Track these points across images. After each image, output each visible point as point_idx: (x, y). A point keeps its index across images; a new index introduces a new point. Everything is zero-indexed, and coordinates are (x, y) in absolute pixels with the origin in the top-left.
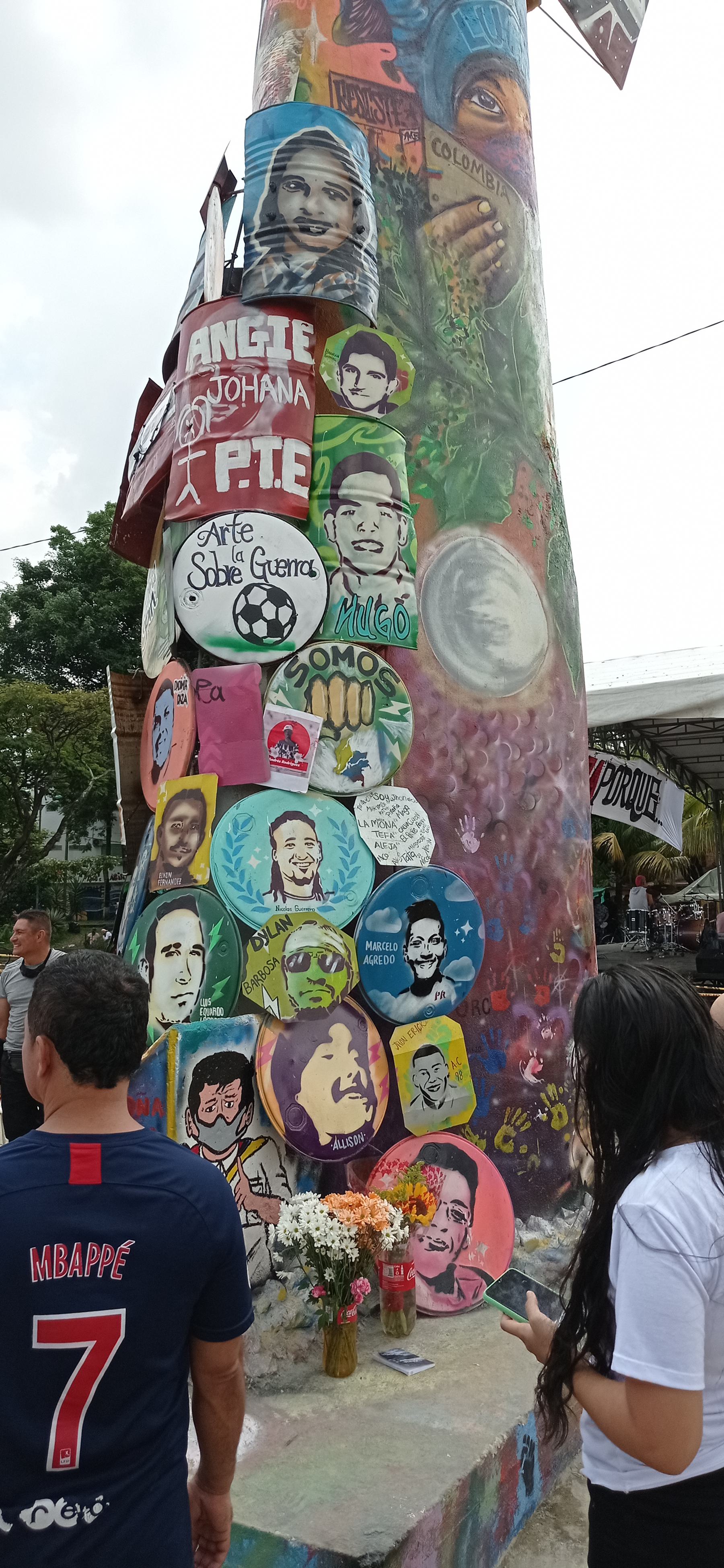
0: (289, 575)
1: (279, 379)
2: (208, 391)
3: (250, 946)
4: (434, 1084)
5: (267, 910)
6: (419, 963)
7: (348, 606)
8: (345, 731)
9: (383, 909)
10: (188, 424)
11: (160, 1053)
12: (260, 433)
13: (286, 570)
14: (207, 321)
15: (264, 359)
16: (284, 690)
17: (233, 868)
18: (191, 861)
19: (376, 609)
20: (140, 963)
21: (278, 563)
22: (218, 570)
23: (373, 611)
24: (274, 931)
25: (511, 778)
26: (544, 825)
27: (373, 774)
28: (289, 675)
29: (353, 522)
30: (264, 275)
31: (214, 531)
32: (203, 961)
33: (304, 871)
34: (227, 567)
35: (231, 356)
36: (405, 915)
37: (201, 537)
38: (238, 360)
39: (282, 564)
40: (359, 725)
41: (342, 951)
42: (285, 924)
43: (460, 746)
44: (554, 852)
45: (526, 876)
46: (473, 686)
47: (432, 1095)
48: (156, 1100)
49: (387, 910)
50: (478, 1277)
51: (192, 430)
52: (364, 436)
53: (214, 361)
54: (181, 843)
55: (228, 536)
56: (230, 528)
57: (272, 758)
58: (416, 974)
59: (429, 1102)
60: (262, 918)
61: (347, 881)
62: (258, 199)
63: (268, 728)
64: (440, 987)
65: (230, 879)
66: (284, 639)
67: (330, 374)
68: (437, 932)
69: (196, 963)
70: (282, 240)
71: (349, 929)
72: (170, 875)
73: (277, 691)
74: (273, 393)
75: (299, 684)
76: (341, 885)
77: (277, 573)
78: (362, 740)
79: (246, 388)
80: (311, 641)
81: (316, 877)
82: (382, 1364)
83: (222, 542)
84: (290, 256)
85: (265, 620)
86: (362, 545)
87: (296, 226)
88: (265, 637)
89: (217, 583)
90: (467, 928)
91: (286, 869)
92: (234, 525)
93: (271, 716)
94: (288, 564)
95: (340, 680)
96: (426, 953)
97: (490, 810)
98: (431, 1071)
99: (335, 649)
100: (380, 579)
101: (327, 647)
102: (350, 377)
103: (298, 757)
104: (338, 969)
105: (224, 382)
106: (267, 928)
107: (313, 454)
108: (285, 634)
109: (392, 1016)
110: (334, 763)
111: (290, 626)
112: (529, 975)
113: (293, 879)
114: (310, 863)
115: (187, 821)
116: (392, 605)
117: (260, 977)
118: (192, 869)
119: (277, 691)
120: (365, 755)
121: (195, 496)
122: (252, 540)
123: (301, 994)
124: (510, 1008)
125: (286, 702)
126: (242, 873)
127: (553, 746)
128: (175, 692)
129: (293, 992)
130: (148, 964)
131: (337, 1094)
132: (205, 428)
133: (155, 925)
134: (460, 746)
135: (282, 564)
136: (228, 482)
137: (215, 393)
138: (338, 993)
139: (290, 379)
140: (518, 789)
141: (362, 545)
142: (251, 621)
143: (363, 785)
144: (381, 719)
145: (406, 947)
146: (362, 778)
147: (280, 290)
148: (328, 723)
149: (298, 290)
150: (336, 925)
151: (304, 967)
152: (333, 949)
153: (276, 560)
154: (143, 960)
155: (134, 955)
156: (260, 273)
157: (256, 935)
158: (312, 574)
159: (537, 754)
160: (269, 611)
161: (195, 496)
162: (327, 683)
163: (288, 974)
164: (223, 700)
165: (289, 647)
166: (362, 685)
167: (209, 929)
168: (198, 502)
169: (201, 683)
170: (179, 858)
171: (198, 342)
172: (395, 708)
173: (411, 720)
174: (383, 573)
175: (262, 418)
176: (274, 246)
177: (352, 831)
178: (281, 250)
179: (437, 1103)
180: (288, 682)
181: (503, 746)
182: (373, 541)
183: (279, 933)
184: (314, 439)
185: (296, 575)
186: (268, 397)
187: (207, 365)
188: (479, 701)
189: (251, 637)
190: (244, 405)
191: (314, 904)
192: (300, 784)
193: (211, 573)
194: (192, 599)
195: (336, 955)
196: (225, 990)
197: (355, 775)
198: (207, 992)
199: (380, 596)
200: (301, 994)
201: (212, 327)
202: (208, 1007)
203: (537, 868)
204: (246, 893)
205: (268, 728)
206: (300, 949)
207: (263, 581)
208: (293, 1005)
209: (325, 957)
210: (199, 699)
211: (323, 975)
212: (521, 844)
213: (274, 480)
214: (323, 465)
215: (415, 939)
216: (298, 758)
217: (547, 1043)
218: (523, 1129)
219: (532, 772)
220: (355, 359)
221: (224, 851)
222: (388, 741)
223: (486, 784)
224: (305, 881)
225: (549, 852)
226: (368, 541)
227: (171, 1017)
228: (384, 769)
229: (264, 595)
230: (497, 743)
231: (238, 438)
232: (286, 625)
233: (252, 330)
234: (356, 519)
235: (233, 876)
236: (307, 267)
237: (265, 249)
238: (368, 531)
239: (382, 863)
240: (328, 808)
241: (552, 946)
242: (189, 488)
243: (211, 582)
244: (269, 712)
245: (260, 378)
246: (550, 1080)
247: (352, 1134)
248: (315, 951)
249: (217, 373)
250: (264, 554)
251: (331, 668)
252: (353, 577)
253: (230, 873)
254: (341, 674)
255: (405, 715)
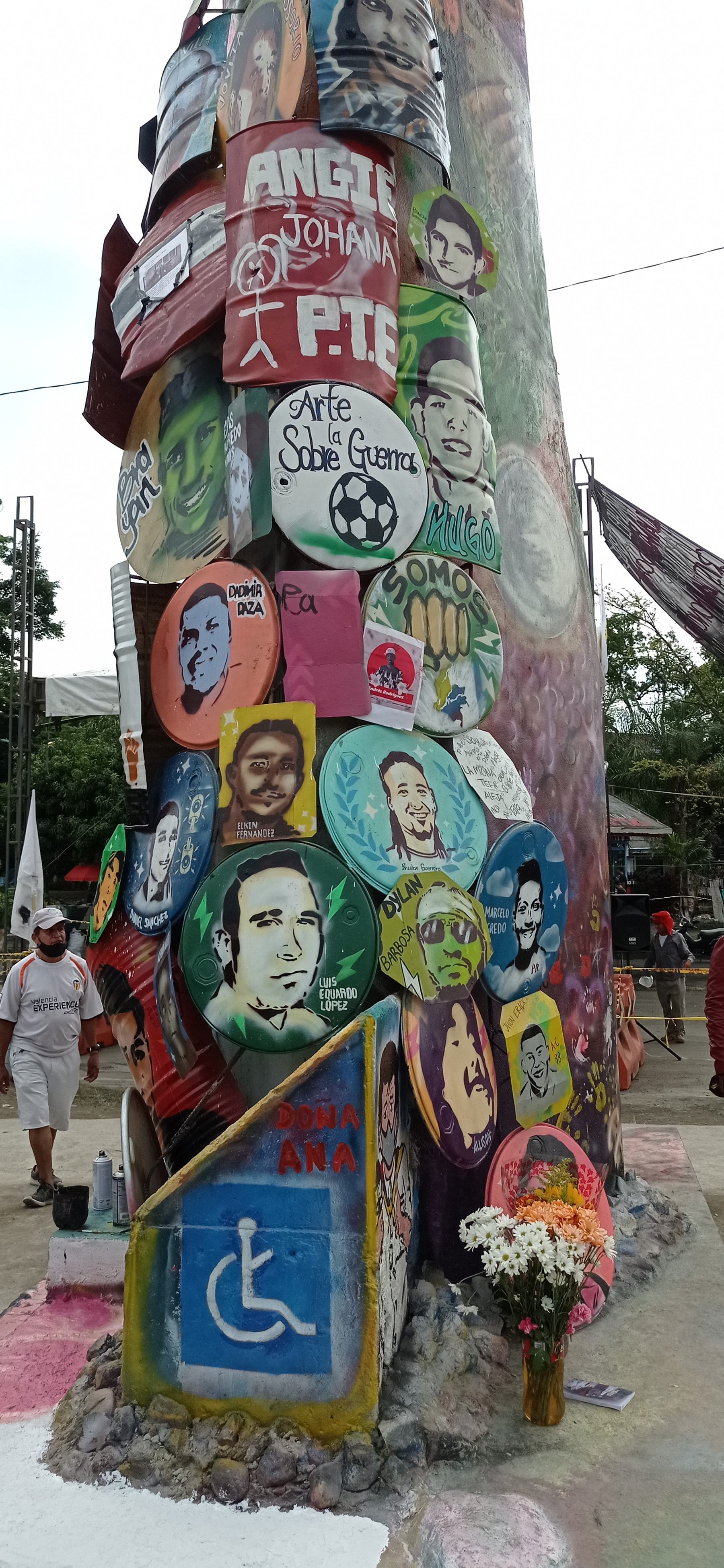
0: (390, 468)
1: (366, 230)
2: (282, 230)
3: (382, 912)
4: (538, 1069)
5: (391, 869)
6: (523, 931)
7: (439, 514)
8: (444, 660)
9: (500, 869)
10: (252, 266)
11: (352, 1047)
12: (347, 291)
13: (387, 461)
14: (274, 144)
15: (349, 203)
16: (383, 605)
17: (350, 818)
18: (287, 807)
19: (466, 522)
20: (216, 936)
21: (378, 452)
22: (314, 451)
23: (463, 523)
24: (405, 895)
25: (559, 727)
26: (583, 782)
27: (471, 712)
28: (387, 587)
29: (443, 417)
30: (348, 102)
31: (307, 402)
32: (320, 931)
33: (423, 823)
34: (323, 448)
35: (309, 192)
36: (516, 876)
37: (293, 406)
38: (319, 199)
39: (382, 454)
40: (456, 655)
41: (473, 918)
42: (415, 885)
43: (518, 689)
44: (590, 811)
45: (570, 836)
46: (527, 624)
47: (539, 1082)
48: (348, 1107)
49: (503, 870)
50: (595, 1283)
51: (260, 275)
52: (452, 318)
53: (288, 194)
54: (267, 785)
55: (324, 410)
56: (326, 401)
57: (372, 686)
58: (520, 945)
59: (535, 1090)
60: (388, 878)
61: (466, 836)
62: (331, 9)
63: (369, 649)
64: (538, 959)
65: (349, 830)
66: (383, 544)
67: (418, 238)
68: (538, 897)
69: (310, 936)
70: (367, 65)
71: (472, 890)
72: (255, 825)
73: (376, 607)
74: (360, 246)
75: (398, 601)
76: (460, 841)
77: (376, 463)
78: (460, 672)
79: (330, 235)
80: (408, 551)
81: (435, 830)
82: (578, 1402)
83: (317, 416)
84: (377, 85)
85: (364, 518)
86: (453, 445)
87: (382, 51)
88: (364, 540)
89: (312, 467)
90: (558, 892)
91: (405, 820)
92: (330, 398)
93: (372, 636)
94: (388, 455)
95: (438, 600)
96: (528, 922)
97: (543, 763)
98: (535, 1054)
99: (431, 562)
100: (468, 486)
101: (423, 558)
102: (438, 245)
103: (402, 688)
104: (472, 940)
105: (303, 223)
106: (398, 890)
107: (399, 328)
108: (385, 538)
109: (499, 994)
110: (434, 698)
111: (390, 529)
112: (576, 945)
113: (413, 832)
114: (427, 814)
115: (276, 760)
116: (480, 519)
117: (397, 951)
118: (290, 818)
119: (376, 607)
120: (462, 690)
121: (269, 357)
122: (349, 419)
123: (440, 969)
124: (563, 982)
125: (386, 620)
126: (361, 823)
127: (587, 698)
128: (229, 600)
129: (432, 967)
130: (229, 937)
131: (469, 1087)
132: (281, 276)
133: (236, 887)
134: (518, 689)
135: (382, 454)
136: (316, 344)
137: (291, 233)
138: (474, 967)
139: (377, 234)
140: (563, 741)
141: (453, 445)
142: (349, 519)
143: (461, 725)
144: (476, 650)
145: (515, 913)
146: (460, 717)
147: (370, 124)
148: (428, 650)
149: (391, 128)
150: (463, 887)
151: (437, 938)
152: (464, 916)
153: (376, 448)
154: (220, 932)
155: (203, 927)
156: (342, 99)
157: (387, 899)
158: (413, 469)
159: (576, 704)
160: (368, 507)
161: (269, 357)
162: (425, 602)
163: (425, 945)
164: (315, 612)
165: (388, 555)
166: (459, 608)
167: (326, 891)
168: (274, 365)
169: (288, 589)
170: (268, 805)
171: (262, 167)
172: (488, 638)
173: (501, 652)
174: (471, 481)
175: (348, 275)
176: (357, 69)
177: (460, 778)
178: (366, 76)
179: (542, 1091)
180: (387, 595)
181: (551, 691)
182: (462, 442)
183: (410, 897)
184: (400, 311)
185: (397, 469)
186: (355, 250)
187: (277, 198)
188: (532, 640)
189: (349, 537)
190: (328, 255)
191: (438, 863)
192: (401, 718)
193: (305, 454)
194: (283, 482)
195: (468, 923)
196: (356, 966)
197: (455, 713)
198: (328, 968)
199: (470, 507)
200: (440, 969)
201: (282, 152)
202: (332, 988)
203: (578, 828)
204: (367, 848)
205: (369, 649)
206: (432, 916)
207: (361, 471)
208: (433, 982)
209: (457, 925)
210: (286, 608)
211: (458, 947)
212: (566, 800)
213: (367, 352)
214: (409, 344)
215: (522, 904)
216: (402, 688)
217: (587, 1018)
218: (576, 1113)
219: (573, 724)
220: (442, 226)
221: (338, 796)
222: (483, 676)
223: (539, 734)
224: (423, 836)
225: (586, 812)
226: (458, 441)
227: (271, 1001)
228: (480, 706)
229: (362, 488)
230: (547, 688)
231: (324, 294)
232: (387, 527)
233: (333, 165)
234: (446, 413)
235: (352, 827)
236: (397, 103)
237: (346, 72)
238: (458, 428)
239: (497, 816)
240: (431, 750)
241: (591, 913)
242: (259, 346)
243: (306, 464)
244: (369, 632)
245: (345, 226)
246: (593, 1060)
247: (484, 1133)
248: (447, 918)
249: (293, 210)
250: (362, 438)
251: (429, 585)
252: (443, 481)
253: (349, 823)
254: (439, 595)
255: (497, 648)
